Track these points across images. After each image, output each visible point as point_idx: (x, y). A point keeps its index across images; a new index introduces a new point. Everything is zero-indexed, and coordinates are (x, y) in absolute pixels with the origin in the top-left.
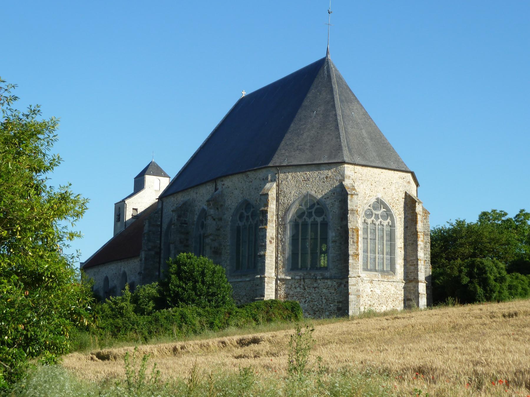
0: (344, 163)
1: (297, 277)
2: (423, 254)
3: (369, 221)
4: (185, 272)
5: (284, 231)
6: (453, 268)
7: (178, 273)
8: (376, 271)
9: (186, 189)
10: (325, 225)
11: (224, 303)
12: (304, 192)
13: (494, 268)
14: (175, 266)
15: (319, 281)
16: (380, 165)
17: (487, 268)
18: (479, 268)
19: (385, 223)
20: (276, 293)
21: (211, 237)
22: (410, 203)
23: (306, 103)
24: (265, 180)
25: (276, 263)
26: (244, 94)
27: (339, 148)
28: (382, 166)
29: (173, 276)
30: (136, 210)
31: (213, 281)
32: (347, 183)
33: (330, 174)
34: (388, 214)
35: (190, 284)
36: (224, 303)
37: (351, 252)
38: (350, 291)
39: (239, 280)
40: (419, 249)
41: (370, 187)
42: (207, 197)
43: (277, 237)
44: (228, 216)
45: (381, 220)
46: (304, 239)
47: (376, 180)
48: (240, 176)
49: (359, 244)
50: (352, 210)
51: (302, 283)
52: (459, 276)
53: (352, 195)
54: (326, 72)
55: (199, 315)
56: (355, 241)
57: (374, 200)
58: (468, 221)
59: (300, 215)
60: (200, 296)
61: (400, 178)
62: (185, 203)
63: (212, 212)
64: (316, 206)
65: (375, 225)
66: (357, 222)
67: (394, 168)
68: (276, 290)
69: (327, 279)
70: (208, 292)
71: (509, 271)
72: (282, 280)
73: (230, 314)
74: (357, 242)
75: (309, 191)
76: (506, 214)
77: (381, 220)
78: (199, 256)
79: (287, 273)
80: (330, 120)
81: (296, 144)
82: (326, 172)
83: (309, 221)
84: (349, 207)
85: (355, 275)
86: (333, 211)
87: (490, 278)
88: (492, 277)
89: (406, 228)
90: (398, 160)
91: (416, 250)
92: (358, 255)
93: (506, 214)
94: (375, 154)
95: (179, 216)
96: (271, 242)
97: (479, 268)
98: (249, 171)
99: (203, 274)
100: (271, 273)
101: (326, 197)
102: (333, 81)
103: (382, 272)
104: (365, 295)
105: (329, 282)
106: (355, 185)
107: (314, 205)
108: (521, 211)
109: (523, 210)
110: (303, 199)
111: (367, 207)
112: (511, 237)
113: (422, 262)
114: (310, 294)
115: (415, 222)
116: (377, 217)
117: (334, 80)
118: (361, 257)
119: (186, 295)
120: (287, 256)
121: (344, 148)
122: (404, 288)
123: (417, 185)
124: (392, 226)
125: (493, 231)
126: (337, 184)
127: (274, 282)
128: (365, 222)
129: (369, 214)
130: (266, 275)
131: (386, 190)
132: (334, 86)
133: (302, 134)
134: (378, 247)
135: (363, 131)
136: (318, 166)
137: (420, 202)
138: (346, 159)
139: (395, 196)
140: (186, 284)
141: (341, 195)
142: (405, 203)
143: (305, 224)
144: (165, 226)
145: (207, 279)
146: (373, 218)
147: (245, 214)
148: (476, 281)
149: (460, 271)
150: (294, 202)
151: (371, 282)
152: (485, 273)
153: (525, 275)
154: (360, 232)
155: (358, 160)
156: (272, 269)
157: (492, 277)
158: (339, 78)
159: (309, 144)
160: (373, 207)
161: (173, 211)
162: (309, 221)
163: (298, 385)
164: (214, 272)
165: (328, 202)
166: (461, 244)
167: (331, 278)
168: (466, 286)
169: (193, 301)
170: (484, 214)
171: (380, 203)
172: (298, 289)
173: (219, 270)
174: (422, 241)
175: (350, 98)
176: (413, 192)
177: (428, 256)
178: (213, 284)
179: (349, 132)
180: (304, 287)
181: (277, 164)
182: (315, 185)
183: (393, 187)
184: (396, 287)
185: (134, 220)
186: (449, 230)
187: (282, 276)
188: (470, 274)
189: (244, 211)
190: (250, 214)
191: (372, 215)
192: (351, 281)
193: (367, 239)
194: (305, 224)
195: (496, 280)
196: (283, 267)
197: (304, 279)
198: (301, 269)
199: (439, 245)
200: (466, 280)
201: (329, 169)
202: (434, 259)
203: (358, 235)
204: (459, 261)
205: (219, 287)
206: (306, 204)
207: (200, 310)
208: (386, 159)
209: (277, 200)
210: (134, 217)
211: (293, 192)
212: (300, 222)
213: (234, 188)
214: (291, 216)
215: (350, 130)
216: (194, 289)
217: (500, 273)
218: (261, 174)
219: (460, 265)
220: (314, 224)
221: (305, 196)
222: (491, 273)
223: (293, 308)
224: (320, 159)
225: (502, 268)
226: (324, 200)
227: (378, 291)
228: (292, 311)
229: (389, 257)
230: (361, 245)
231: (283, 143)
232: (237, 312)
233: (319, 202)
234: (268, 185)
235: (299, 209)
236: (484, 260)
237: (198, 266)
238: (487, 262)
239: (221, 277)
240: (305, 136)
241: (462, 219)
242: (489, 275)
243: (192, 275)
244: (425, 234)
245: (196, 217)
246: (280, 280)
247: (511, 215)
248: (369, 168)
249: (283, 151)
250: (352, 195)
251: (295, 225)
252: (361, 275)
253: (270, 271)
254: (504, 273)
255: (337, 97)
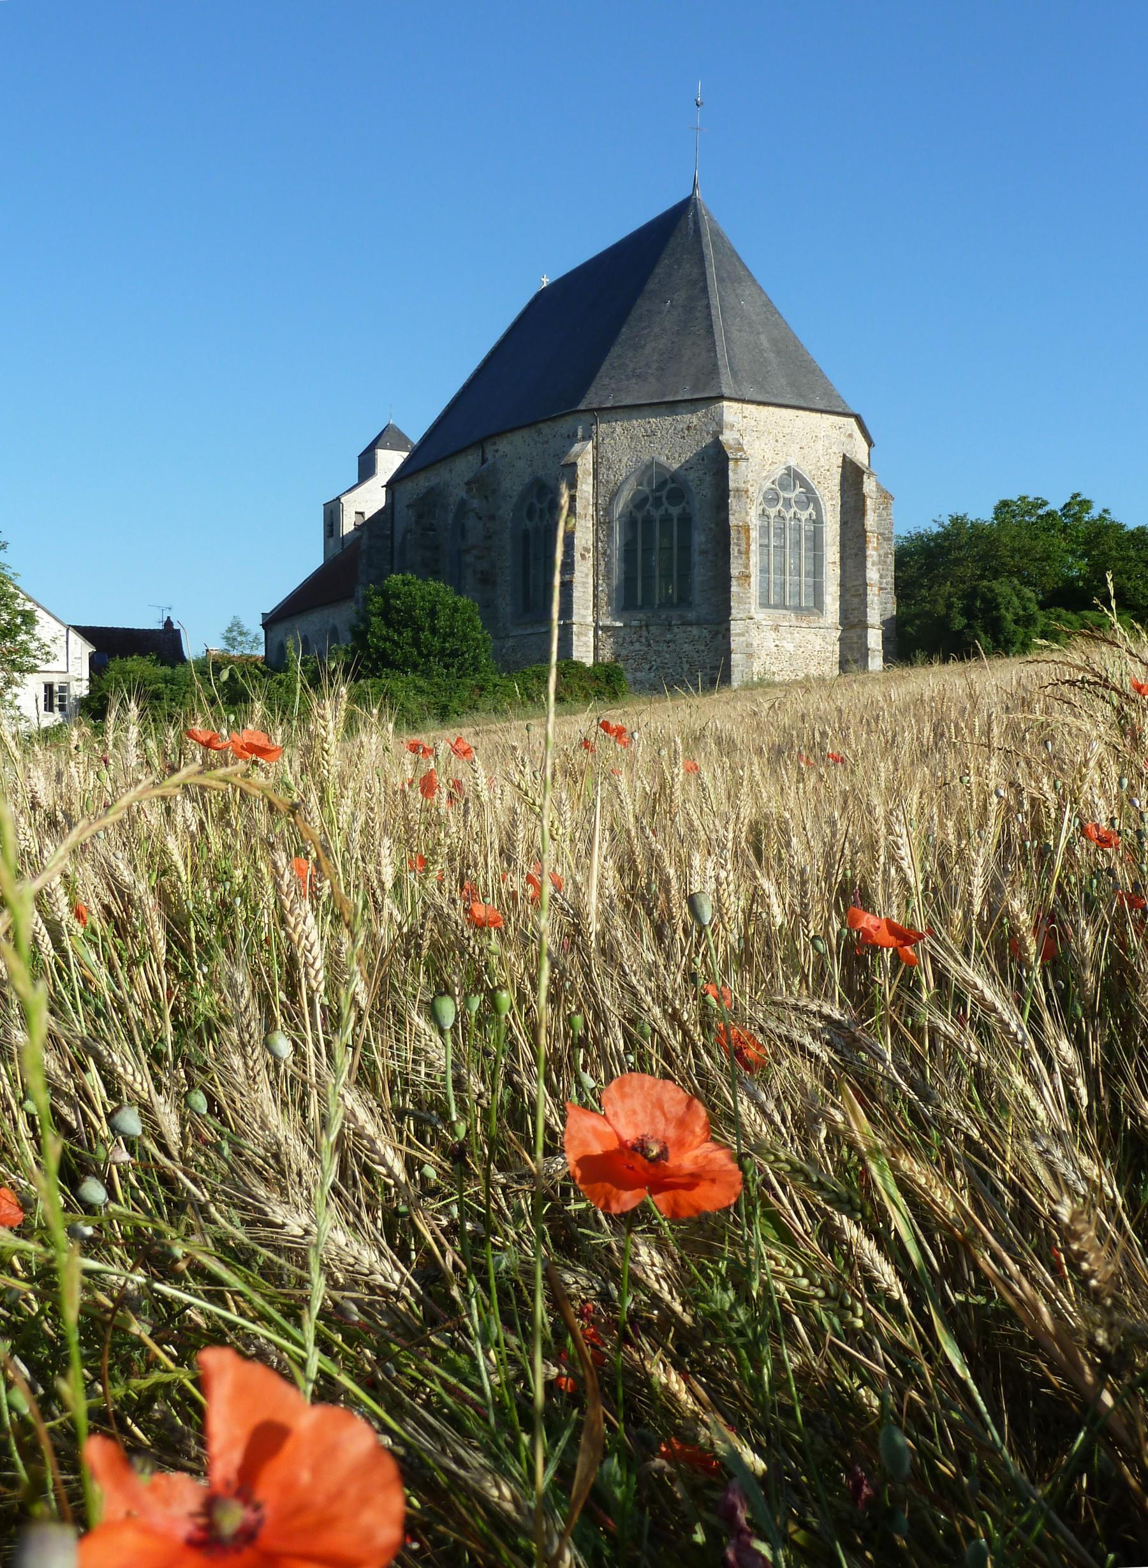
0: (721, 398)
1: (635, 623)
2: (878, 574)
3: (772, 512)
4: (398, 611)
5: (609, 536)
6: (936, 601)
7: (385, 613)
8: (785, 608)
9: (433, 464)
10: (686, 521)
11: (475, 670)
12: (646, 458)
13: (1015, 598)
14: (378, 600)
15: (676, 630)
16: (792, 403)
17: (1000, 600)
18: (984, 600)
19: (804, 515)
20: (596, 655)
21: (474, 552)
22: (852, 475)
23: (652, 285)
24: (572, 438)
25: (595, 596)
26: (546, 281)
27: (714, 370)
28: (797, 403)
29: (373, 619)
30: (362, 514)
31: (452, 627)
32: (727, 437)
33: (695, 421)
34: (811, 498)
35: (408, 634)
36: (475, 670)
37: (734, 572)
38: (733, 646)
39: (529, 631)
40: (869, 564)
41: (775, 446)
42: (468, 476)
43: (596, 548)
44: (506, 511)
45: (794, 509)
46: (648, 550)
47: (787, 430)
48: (525, 433)
49: (752, 555)
50: (738, 490)
51: (644, 633)
52: (947, 616)
53: (737, 460)
54: (691, 225)
55: (420, 691)
56: (743, 549)
57: (780, 471)
58: (971, 518)
59: (639, 502)
60: (427, 656)
61: (833, 426)
62: (431, 491)
63: (475, 503)
64: (670, 486)
65: (784, 518)
66: (747, 514)
67: (821, 407)
68: (596, 648)
69: (691, 624)
70: (444, 649)
71: (1043, 606)
72: (605, 629)
73: (482, 689)
74: (747, 552)
75: (655, 455)
76: (1045, 503)
77: (794, 509)
78: (425, 580)
79: (617, 614)
80: (697, 318)
81: (632, 365)
82: (687, 417)
83: (657, 514)
84: (732, 485)
85: (743, 616)
86: (701, 493)
87: (1005, 618)
88: (1009, 616)
89: (844, 524)
90: (829, 392)
91: (862, 567)
92: (748, 576)
93: (1045, 503)
94: (783, 381)
95: (420, 516)
96: (583, 556)
97: (984, 600)
98: (543, 421)
99: (433, 614)
100: (584, 616)
101: (688, 467)
102: (704, 241)
103: (798, 609)
104: (763, 653)
105: (695, 631)
106: (745, 442)
107: (665, 483)
108: (1075, 497)
109: (1078, 495)
110: (644, 473)
111: (769, 484)
112: (1052, 545)
113: (876, 590)
114: (658, 653)
115: (861, 511)
116: (787, 503)
117: (707, 239)
118: (755, 580)
119: (399, 656)
120: (615, 582)
121: (722, 370)
122: (840, 639)
123: (870, 443)
124: (818, 521)
125: (1019, 535)
126: (709, 440)
127: (591, 633)
128: (764, 514)
129: (772, 498)
130: (575, 619)
131: (806, 450)
132: (706, 251)
133: (643, 347)
134: (790, 562)
135: (763, 337)
136: (672, 407)
137: (871, 474)
138: (726, 392)
139: (822, 462)
140: (400, 634)
141: (716, 460)
142: (843, 477)
143: (648, 521)
144: (398, 538)
145: (441, 623)
146: (779, 507)
147: (538, 506)
148: (978, 624)
149: (950, 606)
150: (627, 478)
151: (776, 628)
152: (997, 607)
153: (1075, 612)
154: (754, 534)
155: (750, 393)
156: (587, 608)
157: (1009, 616)
158: (717, 234)
159: (655, 365)
160: (780, 485)
161: (408, 506)
162: (657, 514)
163: (439, 823)
164: (456, 610)
165: (692, 475)
166: (956, 559)
167: (697, 623)
168: (960, 633)
169: (415, 667)
170: (1005, 504)
171: (792, 477)
172: (637, 646)
173: (464, 607)
174: (875, 549)
175: (737, 272)
176: (860, 453)
177: (890, 579)
178: (452, 634)
179: (733, 339)
180: (647, 640)
181: (594, 406)
182: (668, 443)
183: (819, 445)
184: (824, 638)
185: (358, 534)
186: (938, 534)
187: (606, 621)
188: (968, 612)
189: (535, 501)
190: (545, 505)
191: (778, 500)
192: (735, 627)
193: (768, 546)
194: (648, 521)
195: (1016, 622)
196: (609, 604)
197: (647, 626)
198: (642, 608)
199: (916, 562)
200: (959, 622)
201: (693, 412)
202: (904, 588)
203: (748, 538)
204: (948, 587)
205: (465, 638)
206: (650, 483)
207: (421, 683)
208: (803, 387)
209: (595, 477)
210: (358, 528)
211: (625, 460)
212: (639, 516)
213: (515, 453)
214: (621, 505)
215: (735, 334)
216: (416, 643)
217: (1025, 609)
218: (564, 426)
219: (950, 595)
220: (666, 520)
221: (649, 467)
222: (1007, 609)
223: (608, 676)
224: (676, 393)
225: (1029, 599)
226: (683, 472)
227: (790, 647)
228: (608, 682)
229: (811, 580)
230: (754, 559)
231: (606, 365)
232: (495, 686)
233: (674, 477)
234: (577, 447)
235: (637, 493)
236: (995, 584)
237: (423, 598)
238: (1002, 588)
239: (469, 620)
240: (648, 350)
241: (961, 514)
242: (1003, 611)
243: (411, 617)
244: (884, 537)
245: (451, 515)
246: (602, 628)
247: (1056, 504)
248: (771, 409)
249: (606, 381)
250: (737, 460)
251: (631, 523)
252: (753, 614)
253: (583, 612)
254: (1033, 608)
255: (711, 271)
